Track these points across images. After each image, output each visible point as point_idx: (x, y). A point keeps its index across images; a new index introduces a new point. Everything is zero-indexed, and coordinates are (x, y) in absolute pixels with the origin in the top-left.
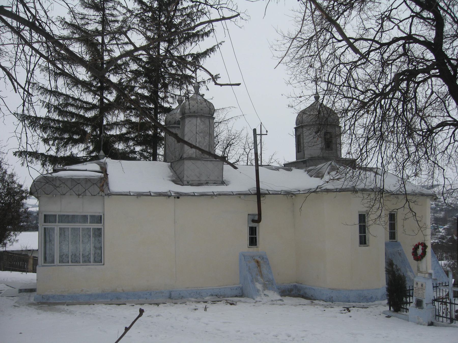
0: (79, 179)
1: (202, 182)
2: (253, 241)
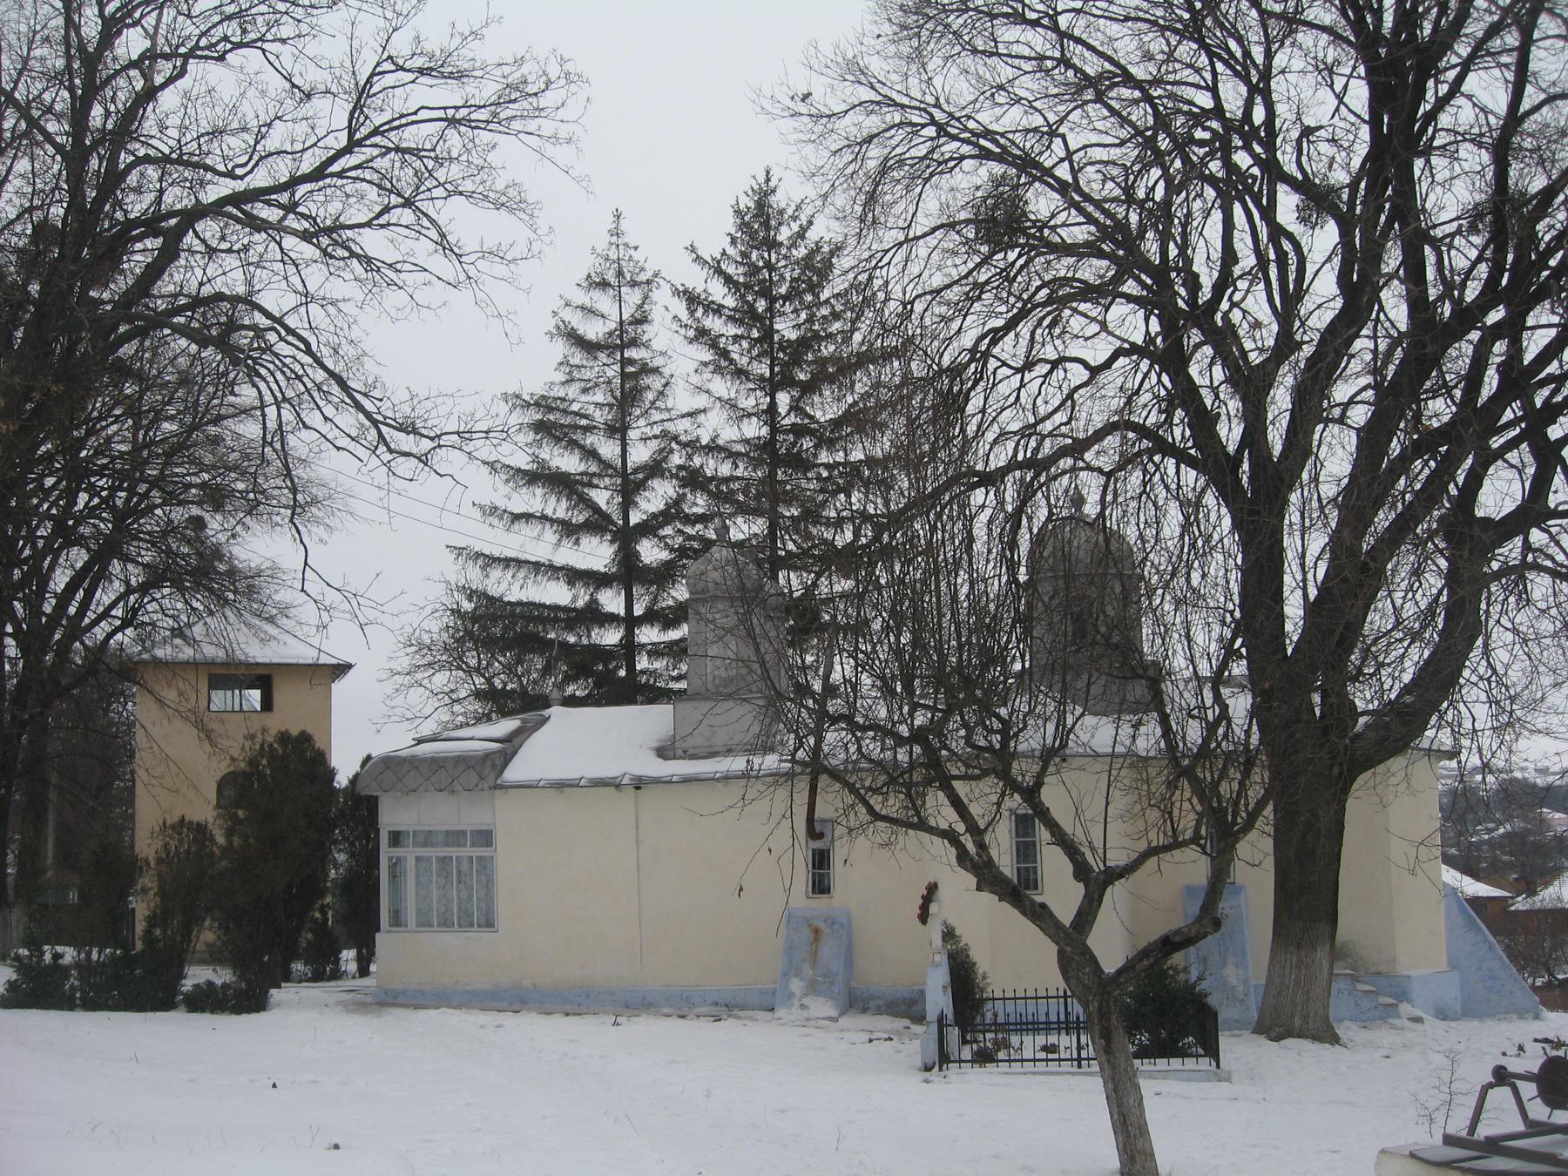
0: (445, 759)
2: (821, 886)
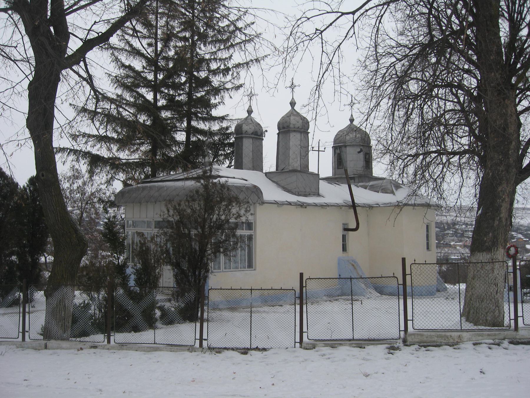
1: (307, 193)
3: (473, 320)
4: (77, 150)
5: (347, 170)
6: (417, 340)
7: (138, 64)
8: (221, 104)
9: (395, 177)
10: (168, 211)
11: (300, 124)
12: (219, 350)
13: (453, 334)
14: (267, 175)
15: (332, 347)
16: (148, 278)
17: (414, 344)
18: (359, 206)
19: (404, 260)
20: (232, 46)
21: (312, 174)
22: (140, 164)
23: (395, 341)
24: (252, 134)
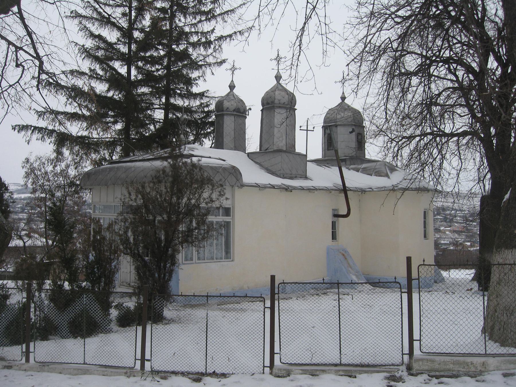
1: (293, 176)
3: (500, 338)
4: (42, 128)
5: (337, 150)
6: (426, 368)
7: (112, 36)
8: (201, 78)
9: (389, 159)
10: (130, 194)
11: (286, 99)
12: (164, 375)
13: (475, 360)
14: (250, 155)
15: (313, 375)
16: (102, 274)
17: (422, 373)
18: (351, 190)
19: (409, 259)
20: (214, 17)
21: (299, 154)
22: (111, 145)
23: (396, 367)
24: (234, 110)
